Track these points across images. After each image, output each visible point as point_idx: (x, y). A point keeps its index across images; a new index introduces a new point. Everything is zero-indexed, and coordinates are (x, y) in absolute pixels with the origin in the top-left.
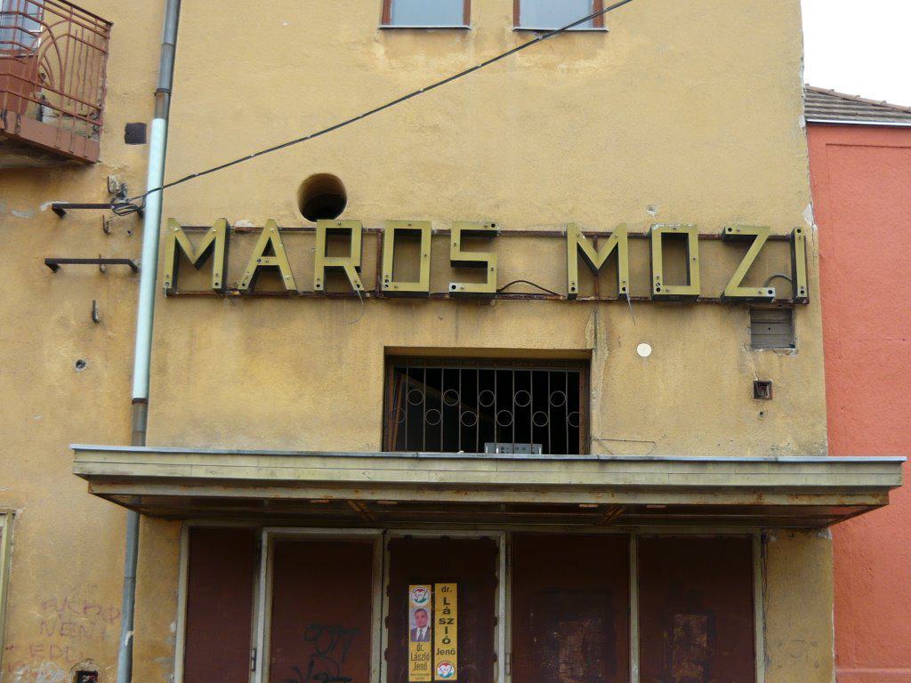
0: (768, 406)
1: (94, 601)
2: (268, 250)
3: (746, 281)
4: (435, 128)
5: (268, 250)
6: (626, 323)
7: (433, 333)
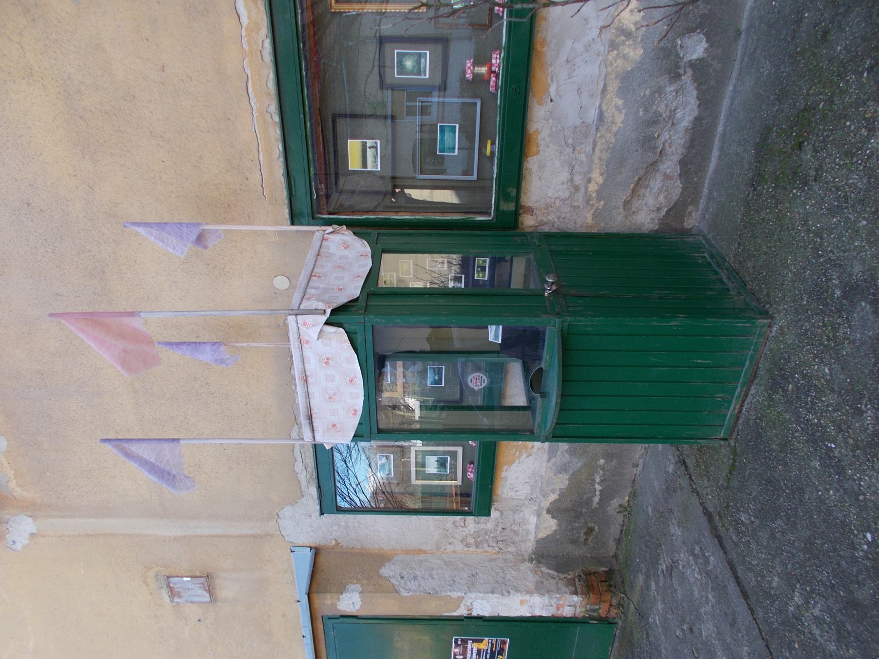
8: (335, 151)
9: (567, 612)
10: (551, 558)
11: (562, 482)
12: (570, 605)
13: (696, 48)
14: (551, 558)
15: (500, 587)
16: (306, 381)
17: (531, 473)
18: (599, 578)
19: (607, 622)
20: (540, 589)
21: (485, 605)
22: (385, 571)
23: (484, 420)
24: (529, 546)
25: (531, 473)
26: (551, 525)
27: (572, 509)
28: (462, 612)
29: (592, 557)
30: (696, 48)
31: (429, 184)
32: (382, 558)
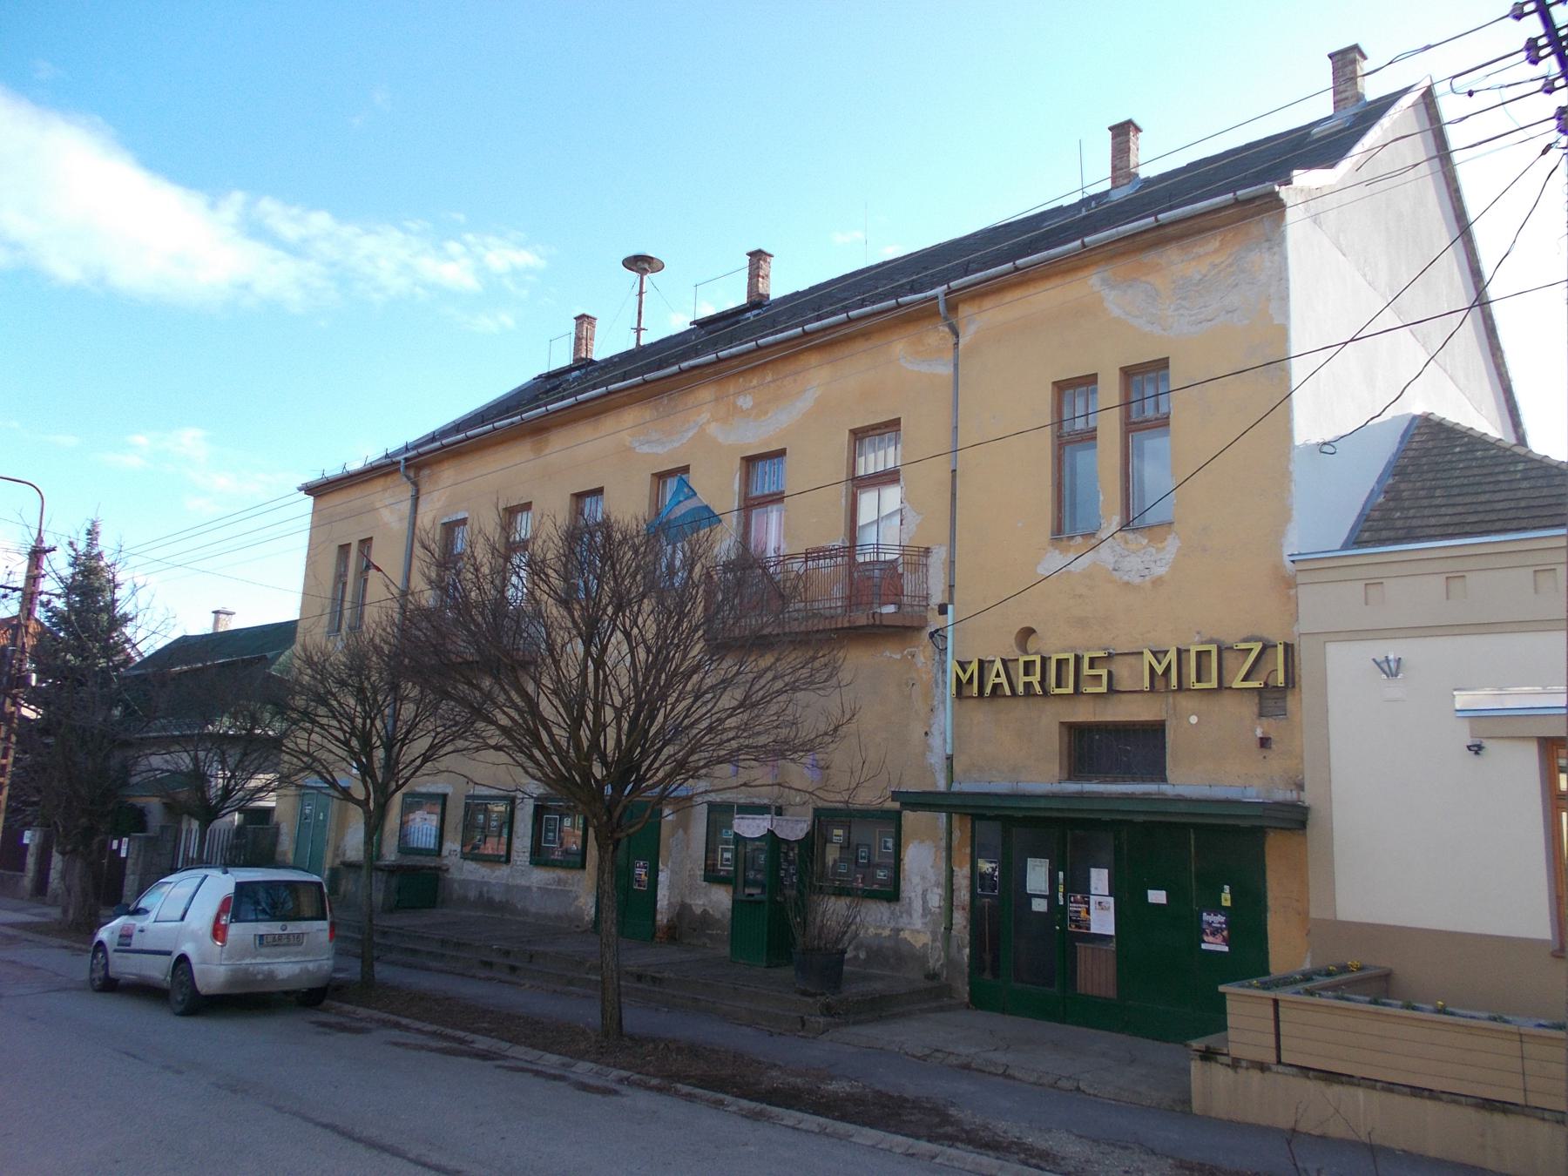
0: (1266, 752)
1: (938, 885)
2: (998, 675)
3: (1245, 679)
4: (1080, 596)
5: (998, 675)
6: (1184, 701)
7: (1084, 713)
8: (404, 1045)
9: (659, 917)
10: (683, 911)
11: (718, 916)
12: (662, 918)
13: (862, 956)
14: (683, 911)
15: (671, 887)
16: (404, 965)
17: (720, 899)
18: (673, 933)
19: (654, 935)
20: (670, 904)
21: (663, 877)
22: (681, 831)
23: (741, 881)
24: (688, 901)
25: (720, 899)
26: (698, 911)
27: (706, 919)
28: (661, 866)
29: (686, 926)
30: (862, 956)
31: (1439, 531)
32: (686, 829)
